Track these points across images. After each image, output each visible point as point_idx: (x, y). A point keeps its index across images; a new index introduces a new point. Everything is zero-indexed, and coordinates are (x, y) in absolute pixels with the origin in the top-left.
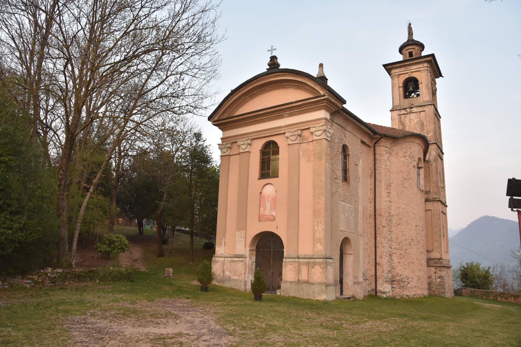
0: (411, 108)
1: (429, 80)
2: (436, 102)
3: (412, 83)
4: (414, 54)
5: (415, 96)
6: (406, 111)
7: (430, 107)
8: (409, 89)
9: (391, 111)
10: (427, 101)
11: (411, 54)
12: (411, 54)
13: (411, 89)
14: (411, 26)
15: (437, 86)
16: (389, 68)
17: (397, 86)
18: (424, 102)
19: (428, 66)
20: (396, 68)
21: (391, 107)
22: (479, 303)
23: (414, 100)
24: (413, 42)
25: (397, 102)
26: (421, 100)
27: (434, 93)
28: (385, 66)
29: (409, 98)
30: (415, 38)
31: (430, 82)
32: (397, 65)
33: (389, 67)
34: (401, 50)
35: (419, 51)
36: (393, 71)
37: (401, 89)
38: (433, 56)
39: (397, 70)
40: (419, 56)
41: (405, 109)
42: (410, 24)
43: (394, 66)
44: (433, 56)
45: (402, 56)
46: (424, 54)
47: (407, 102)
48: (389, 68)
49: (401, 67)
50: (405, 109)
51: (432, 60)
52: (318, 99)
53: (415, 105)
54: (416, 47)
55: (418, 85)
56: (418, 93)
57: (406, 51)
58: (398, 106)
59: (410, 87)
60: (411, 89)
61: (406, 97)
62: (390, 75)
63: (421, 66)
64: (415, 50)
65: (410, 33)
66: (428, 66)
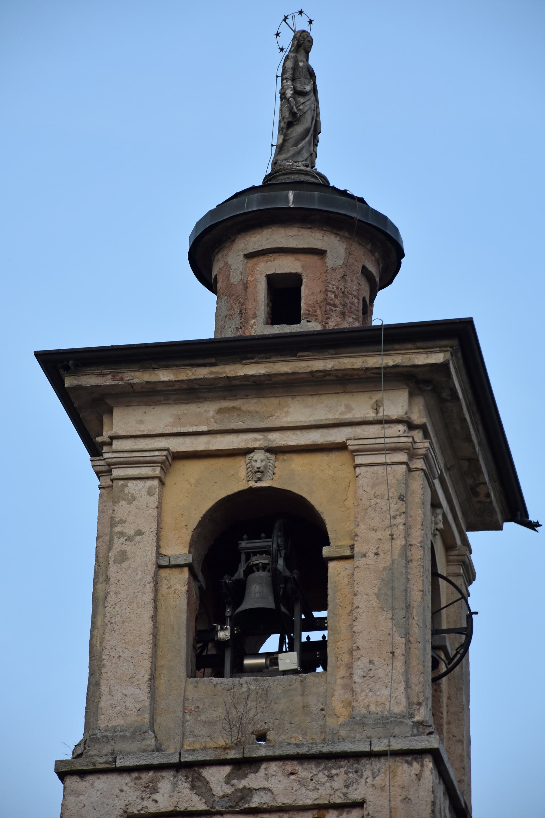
0: (246, 764)
1: (417, 535)
2: (464, 741)
3: (274, 542)
4: (308, 295)
5: (289, 660)
6: (200, 786)
7: (406, 771)
8: (240, 590)
9: (64, 772)
10: (386, 722)
11: (284, 296)
12: (284, 296)
13: (258, 595)
14: (315, 59)
15: (478, 596)
16: (89, 382)
17: (143, 555)
18: (357, 722)
19: (418, 416)
20: (152, 395)
21: (67, 735)
22: (446, 478)
23: (276, 697)
24: (315, 201)
25: (129, 699)
26: (337, 703)
27: (447, 651)
28: (56, 365)
29: (239, 669)
30: (338, 164)
31: (419, 556)
32: (165, 376)
33: (90, 380)
34: (206, 252)
35: (358, 286)
36: (123, 422)
37: (178, 583)
38: (460, 335)
39: (159, 418)
40: (351, 323)
41: (188, 768)
42: (302, 43)
43: (139, 377)
44: (460, 335)
45: (214, 297)
46: (391, 307)
47: (209, 711)
48: (89, 382)
49: (191, 392)
50: (188, 768)
51: (450, 368)
52: (202, 373)
53: (284, 740)
54: (335, 247)
55: (322, 566)
56: (316, 636)
57: (248, 265)
58: (137, 733)
59: (254, 574)
60: (258, 595)
61: (209, 658)
62: (94, 449)
63: (360, 406)
64: (326, 266)
65: (299, 118)
66: (418, 416)
